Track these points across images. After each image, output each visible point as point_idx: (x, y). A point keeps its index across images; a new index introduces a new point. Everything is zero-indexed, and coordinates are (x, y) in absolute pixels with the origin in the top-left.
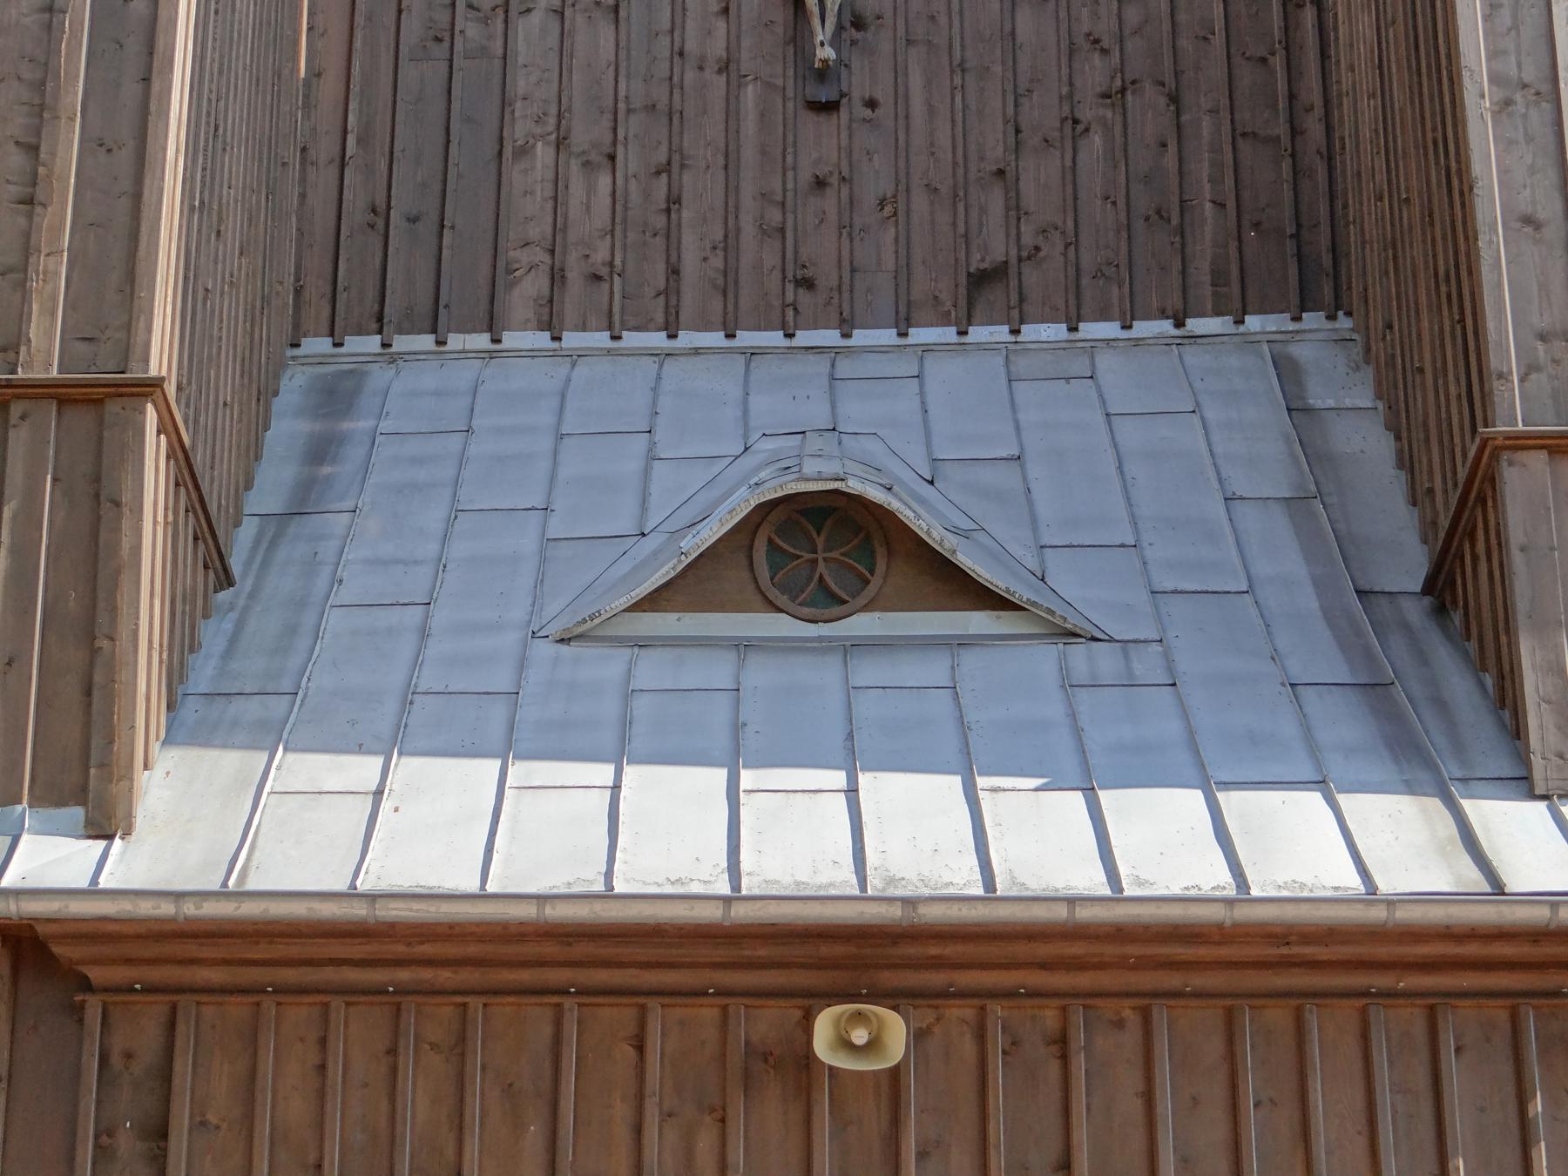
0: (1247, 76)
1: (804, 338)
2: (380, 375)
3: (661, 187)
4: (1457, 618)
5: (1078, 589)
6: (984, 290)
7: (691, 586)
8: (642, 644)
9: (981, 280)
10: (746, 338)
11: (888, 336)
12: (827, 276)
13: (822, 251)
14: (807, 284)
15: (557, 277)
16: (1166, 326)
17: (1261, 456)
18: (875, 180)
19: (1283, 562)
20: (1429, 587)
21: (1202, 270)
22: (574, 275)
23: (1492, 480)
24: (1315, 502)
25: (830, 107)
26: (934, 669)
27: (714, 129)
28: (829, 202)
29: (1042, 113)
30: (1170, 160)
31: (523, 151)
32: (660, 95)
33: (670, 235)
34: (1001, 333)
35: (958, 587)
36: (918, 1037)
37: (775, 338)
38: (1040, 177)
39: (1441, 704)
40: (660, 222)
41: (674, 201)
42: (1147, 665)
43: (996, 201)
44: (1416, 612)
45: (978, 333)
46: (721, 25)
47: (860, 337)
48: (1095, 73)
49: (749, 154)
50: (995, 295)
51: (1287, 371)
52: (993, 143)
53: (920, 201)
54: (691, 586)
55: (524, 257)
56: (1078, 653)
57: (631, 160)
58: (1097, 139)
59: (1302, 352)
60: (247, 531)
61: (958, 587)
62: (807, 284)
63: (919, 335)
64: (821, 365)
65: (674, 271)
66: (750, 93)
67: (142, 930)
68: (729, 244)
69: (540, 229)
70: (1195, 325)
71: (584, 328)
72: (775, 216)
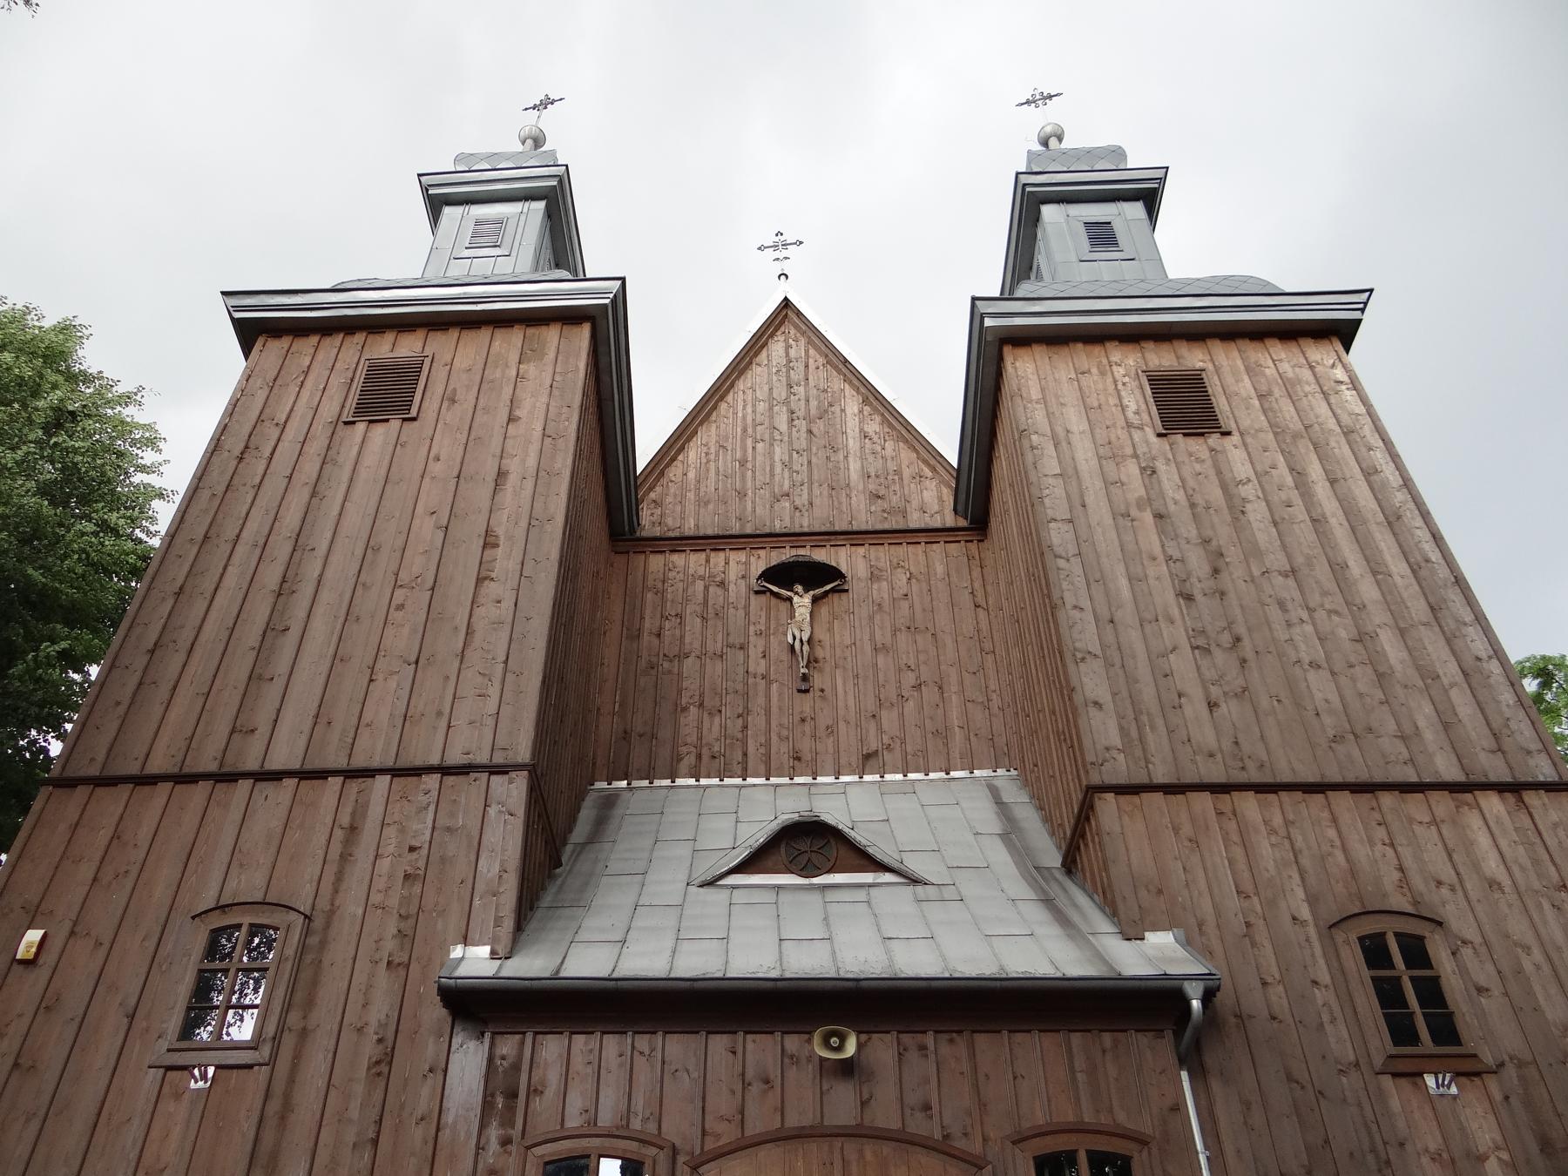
0: (968, 678)
1: (798, 780)
2: (627, 795)
3: (740, 721)
4: (1079, 874)
5: (914, 865)
6: (868, 761)
7: (754, 862)
8: (734, 887)
9: (867, 757)
10: (773, 780)
11: (831, 779)
12: (807, 756)
13: (805, 746)
14: (799, 759)
15: (699, 757)
16: (942, 775)
17: (984, 815)
18: (824, 720)
19: (1000, 856)
20: (1064, 864)
21: (955, 754)
22: (705, 758)
23: (1092, 807)
24: (1011, 834)
25: (807, 691)
26: (861, 895)
27: (761, 700)
28: (807, 728)
29: (891, 692)
30: (940, 711)
31: (685, 709)
32: (740, 687)
33: (745, 743)
34: (877, 777)
35: (867, 861)
36: (860, 1046)
37: (786, 780)
38: (889, 719)
39: (1076, 906)
40: (740, 736)
41: (745, 727)
42: (949, 893)
43: (872, 727)
44: (1060, 876)
45: (867, 778)
46: (763, 662)
47: (820, 779)
48: (910, 679)
49: (774, 709)
50: (872, 762)
51: (994, 792)
52: (870, 704)
53: (842, 725)
54: (754, 862)
55: (684, 750)
56: (919, 888)
57: (728, 712)
58: (911, 703)
59: (997, 783)
60: (569, 848)
61: (867, 861)
62: (799, 759)
63: (844, 779)
64: (805, 789)
65: (745, 755)
66: (775, 686)
67: (592, 418)
68: (768, 744)
69: (693, 739)
70: (954, 774)
71: (709, 777)
72: (785, 733)
